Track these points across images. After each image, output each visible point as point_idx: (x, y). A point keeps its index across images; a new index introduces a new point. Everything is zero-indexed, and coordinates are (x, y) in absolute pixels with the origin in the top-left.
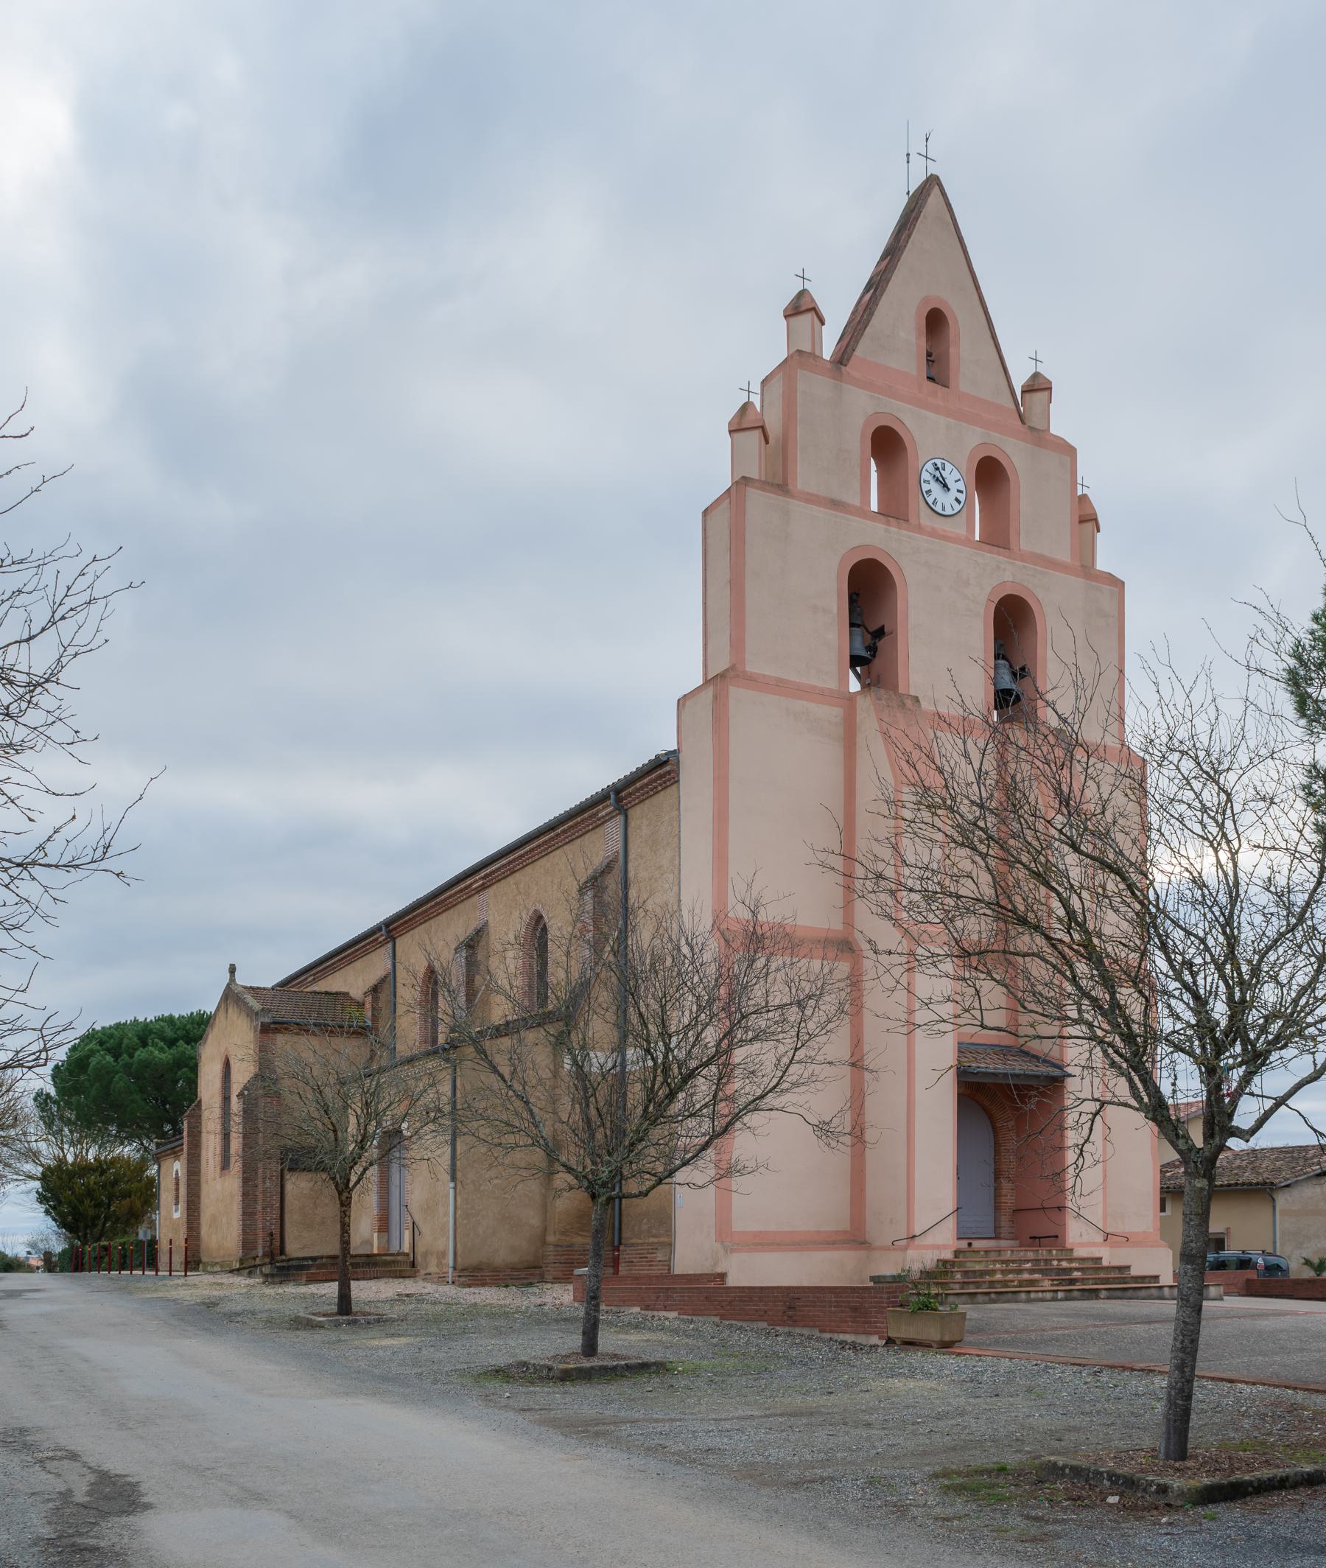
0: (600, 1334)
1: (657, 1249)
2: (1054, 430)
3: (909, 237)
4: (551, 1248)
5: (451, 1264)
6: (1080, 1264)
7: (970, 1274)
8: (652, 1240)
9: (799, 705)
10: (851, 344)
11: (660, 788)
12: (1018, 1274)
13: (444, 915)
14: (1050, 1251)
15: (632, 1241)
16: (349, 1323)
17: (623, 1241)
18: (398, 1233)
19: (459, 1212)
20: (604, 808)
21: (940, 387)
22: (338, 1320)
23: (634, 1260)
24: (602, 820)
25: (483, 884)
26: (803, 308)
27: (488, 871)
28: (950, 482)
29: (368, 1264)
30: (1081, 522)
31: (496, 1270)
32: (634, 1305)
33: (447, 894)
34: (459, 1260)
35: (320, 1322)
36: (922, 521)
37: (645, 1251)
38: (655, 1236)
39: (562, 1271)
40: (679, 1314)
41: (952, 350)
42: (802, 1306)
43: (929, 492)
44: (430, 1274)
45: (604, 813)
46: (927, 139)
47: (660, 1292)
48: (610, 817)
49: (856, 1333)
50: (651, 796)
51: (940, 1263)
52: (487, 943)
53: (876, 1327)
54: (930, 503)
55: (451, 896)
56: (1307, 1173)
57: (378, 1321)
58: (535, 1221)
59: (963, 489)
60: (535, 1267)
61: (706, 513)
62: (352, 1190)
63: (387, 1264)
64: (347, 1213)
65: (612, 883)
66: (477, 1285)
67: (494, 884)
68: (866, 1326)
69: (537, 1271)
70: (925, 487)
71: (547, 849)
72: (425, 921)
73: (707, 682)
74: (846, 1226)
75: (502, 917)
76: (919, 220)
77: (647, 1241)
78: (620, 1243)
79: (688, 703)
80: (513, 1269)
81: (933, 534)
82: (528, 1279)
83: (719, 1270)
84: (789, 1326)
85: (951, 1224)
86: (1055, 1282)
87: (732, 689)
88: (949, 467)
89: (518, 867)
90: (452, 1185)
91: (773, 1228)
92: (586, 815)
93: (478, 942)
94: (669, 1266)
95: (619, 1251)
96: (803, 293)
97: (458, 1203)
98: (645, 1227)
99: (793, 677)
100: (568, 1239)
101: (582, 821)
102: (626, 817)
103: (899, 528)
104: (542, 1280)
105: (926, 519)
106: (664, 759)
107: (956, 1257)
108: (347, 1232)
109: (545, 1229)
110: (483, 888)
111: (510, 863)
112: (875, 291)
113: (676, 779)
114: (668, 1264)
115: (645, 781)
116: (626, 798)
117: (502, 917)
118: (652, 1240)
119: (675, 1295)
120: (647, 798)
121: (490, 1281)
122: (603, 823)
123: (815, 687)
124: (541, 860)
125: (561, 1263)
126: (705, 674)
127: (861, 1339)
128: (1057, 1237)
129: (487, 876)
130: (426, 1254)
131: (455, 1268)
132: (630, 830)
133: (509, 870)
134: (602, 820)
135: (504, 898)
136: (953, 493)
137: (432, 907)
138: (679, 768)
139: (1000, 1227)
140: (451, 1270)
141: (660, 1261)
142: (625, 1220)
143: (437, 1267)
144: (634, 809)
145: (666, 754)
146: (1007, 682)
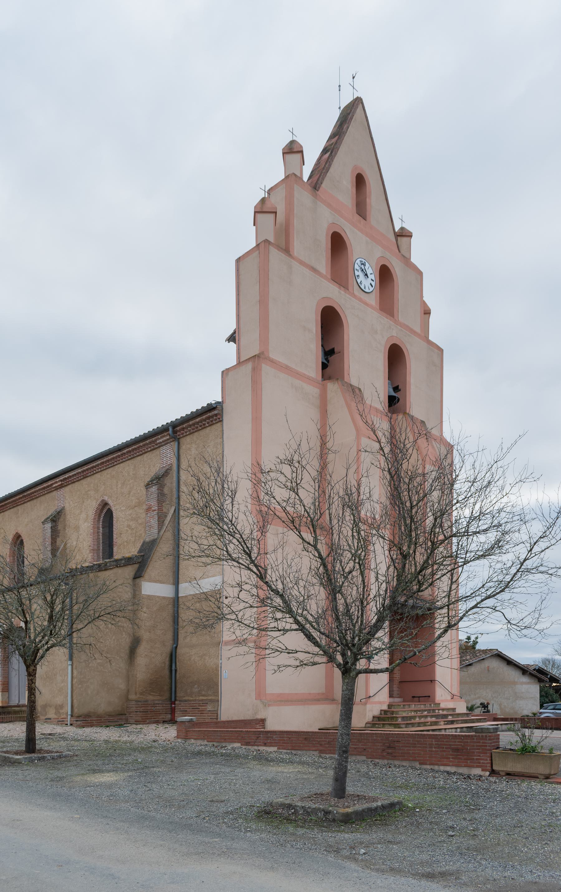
0: (24, 735)
1: (207, 703)
2: (413, 260)
3: (348, 128)
4: (134, 703)
5: (69, 713)
6: (447, 712)
7: (405, 718)
8: (201, 698)
9: (297, 382)
10: (320, 179)
11: (214, 422)
12: (426, 718)
13: (28, 503)
14: (431, 705)
15: (184, 698)
16: (39, 759)
17: (177, 698)
18: (17, 692)
19: (75, 680)
20: (161, 437)
21: (362, 219)
22: (32, 757)
23: (188, 710)
24: (159, 445)
25: (62, 484)
26: (295, 150)
27: (66, 476)
28: (369, 275)
29: (4, 713)
30: (425, 314)
31: (99, 716)
32: (235, 742)
33: (33, 490)
34: (76, 710)
35: (18, 759)
36: (355, 292)
37: (197, 705)
38: (204, 696)
39: (141, 717)
40: (278, 749)
41: (368, 200)
42: (402, 746)
43: (358, 276)
44: (50, 719)
45: (161, 440)
46: (354, 78)
47: (260, 734)
48: (166, 443)
49: (457, 766)
50: (200, 430)
51: (383, 712)
52: (64, 520)
53: (480, 763)
54: (359, 283)
55: (35, 492)
56: (463, 664)
57: (60, 757)
58: (123, 686)
59: (374, 279)
60: (122, 715)
61: (238, 261)
62: (37, 664)
63: (16, 712)
64: (34, 681)
65: (170, 483)
66: (88, 726)
67: (69, 484)
68: (469, 761)
69: (124, 717)
70: (357, 273)
71: (108, 465)
72: (14, 507)
73: (240, 363)
74: (323, 690)
75: (76, 504)
76: (353, 120)
77: (197, 699)
78: (175, 700)
79: (230, 373)
80: (110, 716)
81: (360, 300)
82: (118, 722)
83: (259, 717)
84: (388, 759)
85: (386, 690)
86: (446, 723)
87: (263, 365)
88: (367, 264)
89: (90, 474)
90: (70, 663)
91: (287, 691)
92: (147, 442)
93: (59, 519)
94: (217, 714)
95: (175, 704)
96: (292, 142)
97: (75, 674)
98: (196, 690)
99: (293, 366)
100: (144, 697)
101: (144, 445)
102: (179, 443)
103: (345, 293)
104: (127, 722)
105: (357, 292)
106: (215, 406)
107: (389, 708)
108: (34, 695)
109: (128, 691)
110: (61, 486)
111: (83, 472)
112: (331, 153)
113: (221, 419)
114: (216, 713)
115: (197, 420)
116: (180, 431)
117: (76, 504)
118: (201, 698)
119: (274, 736)
120: (196, 431)
121: (96, 723)
122: (159, 447)
123: (304, 374)
124: (108, 470)
125: (140, 712)
126: (239, 357)
127: (464, 770)
128: (429, 696)
129: (65, 479)
130: (45, 707)
131: (72, 716)
132: (181, 451)
133: (83, 476)
134: (159, 445)
135: (78, 493)
136: (369, 281)
137: (20, 498)
138: (222, 412)
139: (393, 691)
140: (69, 717)
141: (209, 711)
142: (179, 685)
143: (56, 714)
144: (185, 438)
145: (215, 403)
146: (393, 394)
